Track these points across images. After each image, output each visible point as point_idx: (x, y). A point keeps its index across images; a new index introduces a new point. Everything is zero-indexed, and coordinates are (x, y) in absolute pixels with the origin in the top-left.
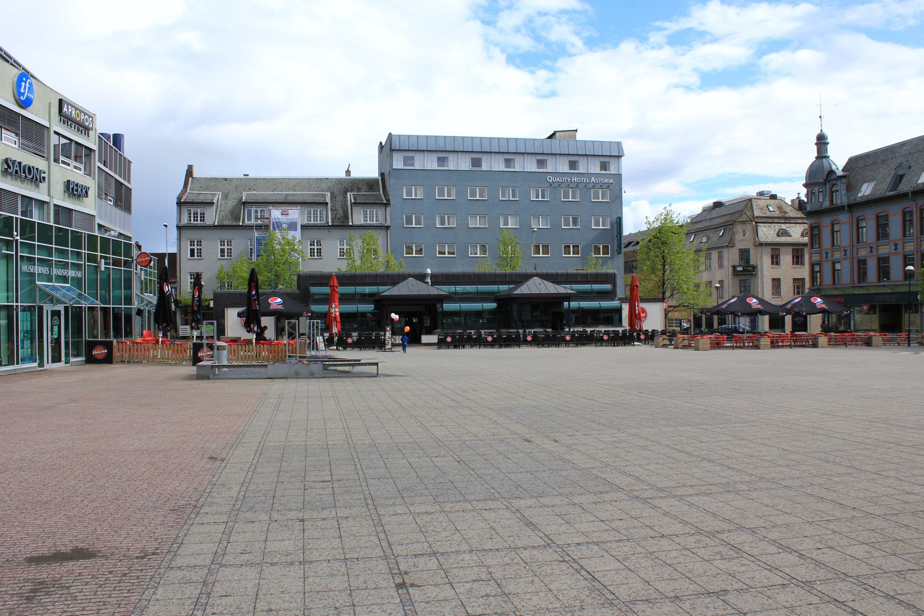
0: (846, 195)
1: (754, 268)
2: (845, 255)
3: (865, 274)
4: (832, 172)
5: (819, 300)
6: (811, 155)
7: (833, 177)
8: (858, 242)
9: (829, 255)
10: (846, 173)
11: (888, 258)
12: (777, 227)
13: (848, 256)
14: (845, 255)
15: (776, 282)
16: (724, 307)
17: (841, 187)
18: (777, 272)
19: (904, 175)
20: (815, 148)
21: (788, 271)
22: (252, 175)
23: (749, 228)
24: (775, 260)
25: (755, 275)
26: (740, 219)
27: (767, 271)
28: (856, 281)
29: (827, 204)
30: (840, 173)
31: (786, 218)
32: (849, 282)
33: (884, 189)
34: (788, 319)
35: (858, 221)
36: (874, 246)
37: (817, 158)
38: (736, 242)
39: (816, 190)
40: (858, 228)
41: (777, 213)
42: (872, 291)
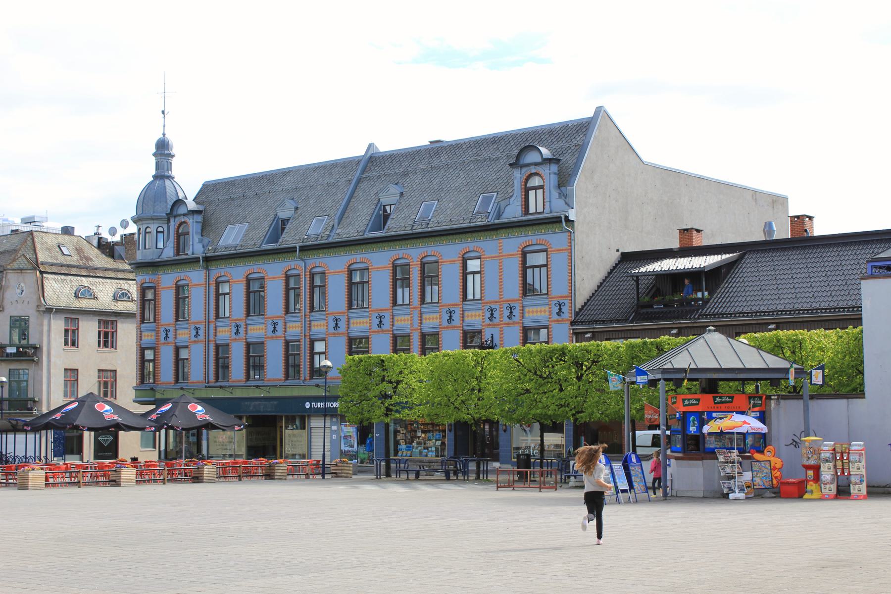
0: (201, 241)
1: (37, 349)
2: (197, 335)
3: (226, 367)
4: (179, 202)
5: (200, 408)
6: (148, 170)
7: (182, 210)
8: (217, 316)
9: (171, 335)
10: (201, 208)
11: (263, 343)
12: (76, 282)
13: (202, 337)
14: (197, 335)
15: (72, 374)
16: (58, 416)
17: (193, 225)
18: (108, 359)
19: (288, 220)
20: (153, 161)
21: (89, 358)
22: (385, 146)
23: (31, 278)
24: (71, 339)
25: (38, 363)
26: (15, 265)
27: (57, 357)
28: (212, 378)
29: (169, 253)
30: (191, 205)
31: (88, 268)
32: (201, 379)
33: (258, 240)
34: (88, 438)
35: (218, 284)
36: (243, 324)
37: (156, 177)
38: (6, 303)
39: (153, 228)
40: (218, 295)
41: (74, 260)
42: (238, 394)
